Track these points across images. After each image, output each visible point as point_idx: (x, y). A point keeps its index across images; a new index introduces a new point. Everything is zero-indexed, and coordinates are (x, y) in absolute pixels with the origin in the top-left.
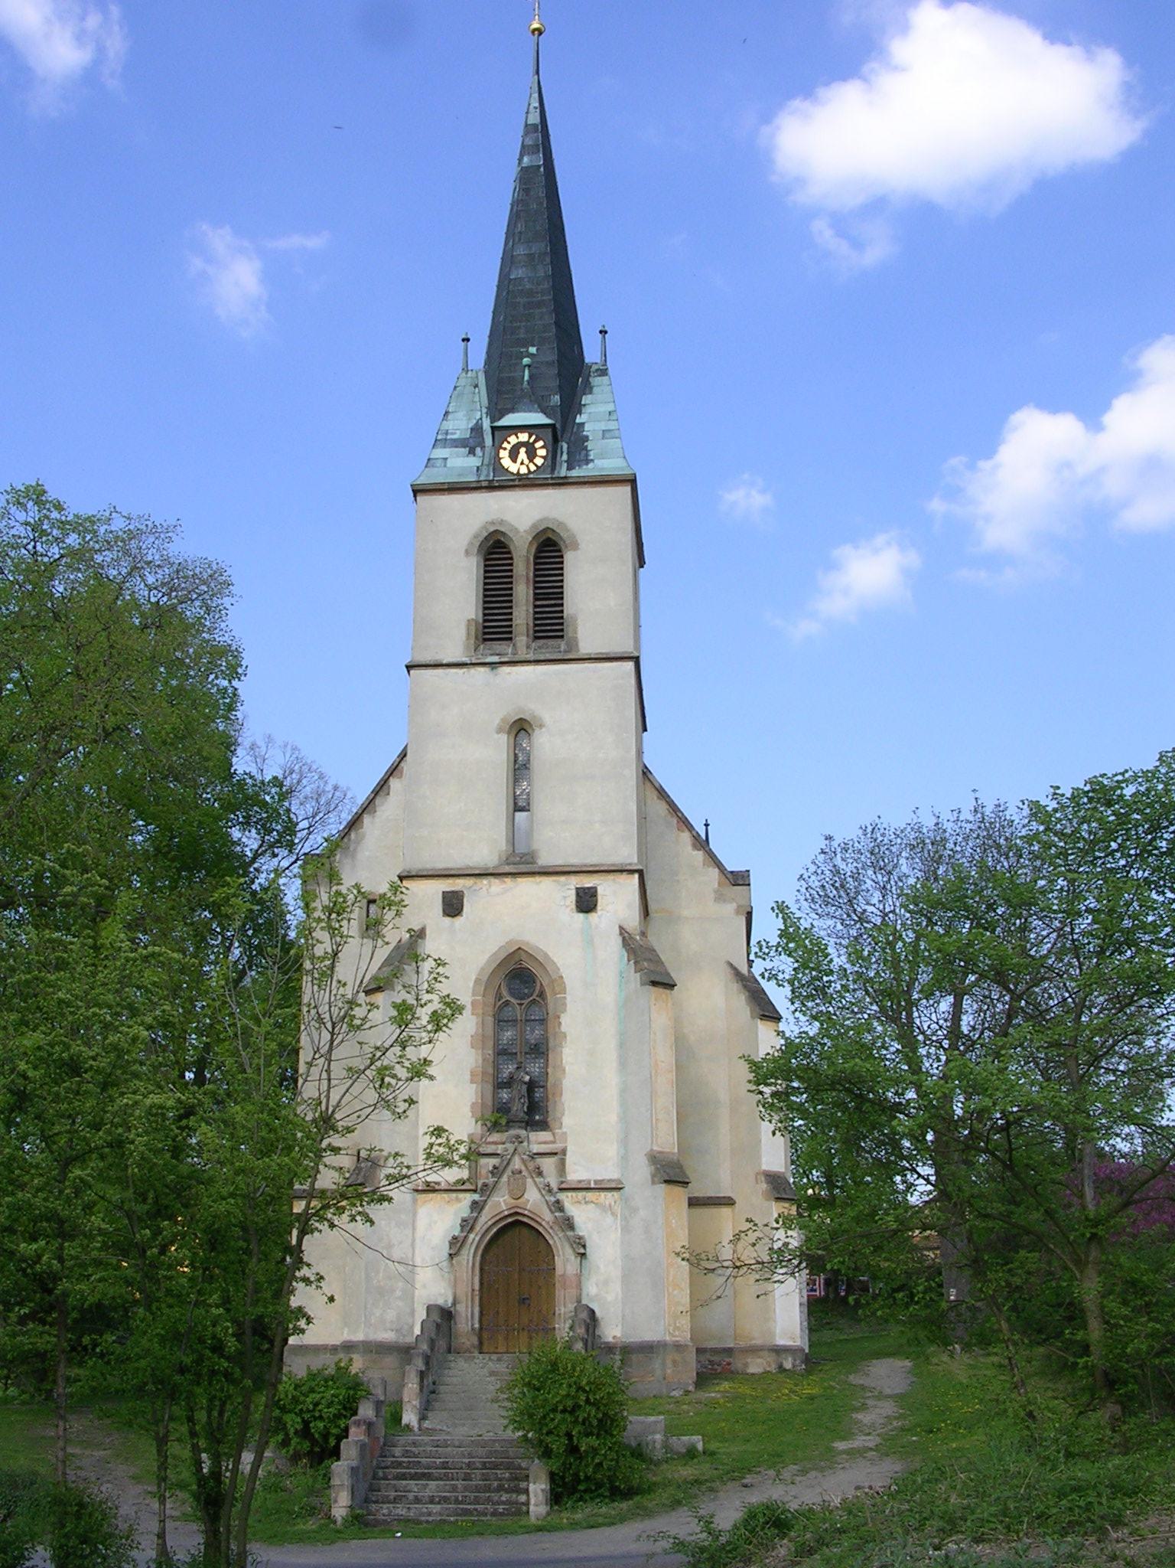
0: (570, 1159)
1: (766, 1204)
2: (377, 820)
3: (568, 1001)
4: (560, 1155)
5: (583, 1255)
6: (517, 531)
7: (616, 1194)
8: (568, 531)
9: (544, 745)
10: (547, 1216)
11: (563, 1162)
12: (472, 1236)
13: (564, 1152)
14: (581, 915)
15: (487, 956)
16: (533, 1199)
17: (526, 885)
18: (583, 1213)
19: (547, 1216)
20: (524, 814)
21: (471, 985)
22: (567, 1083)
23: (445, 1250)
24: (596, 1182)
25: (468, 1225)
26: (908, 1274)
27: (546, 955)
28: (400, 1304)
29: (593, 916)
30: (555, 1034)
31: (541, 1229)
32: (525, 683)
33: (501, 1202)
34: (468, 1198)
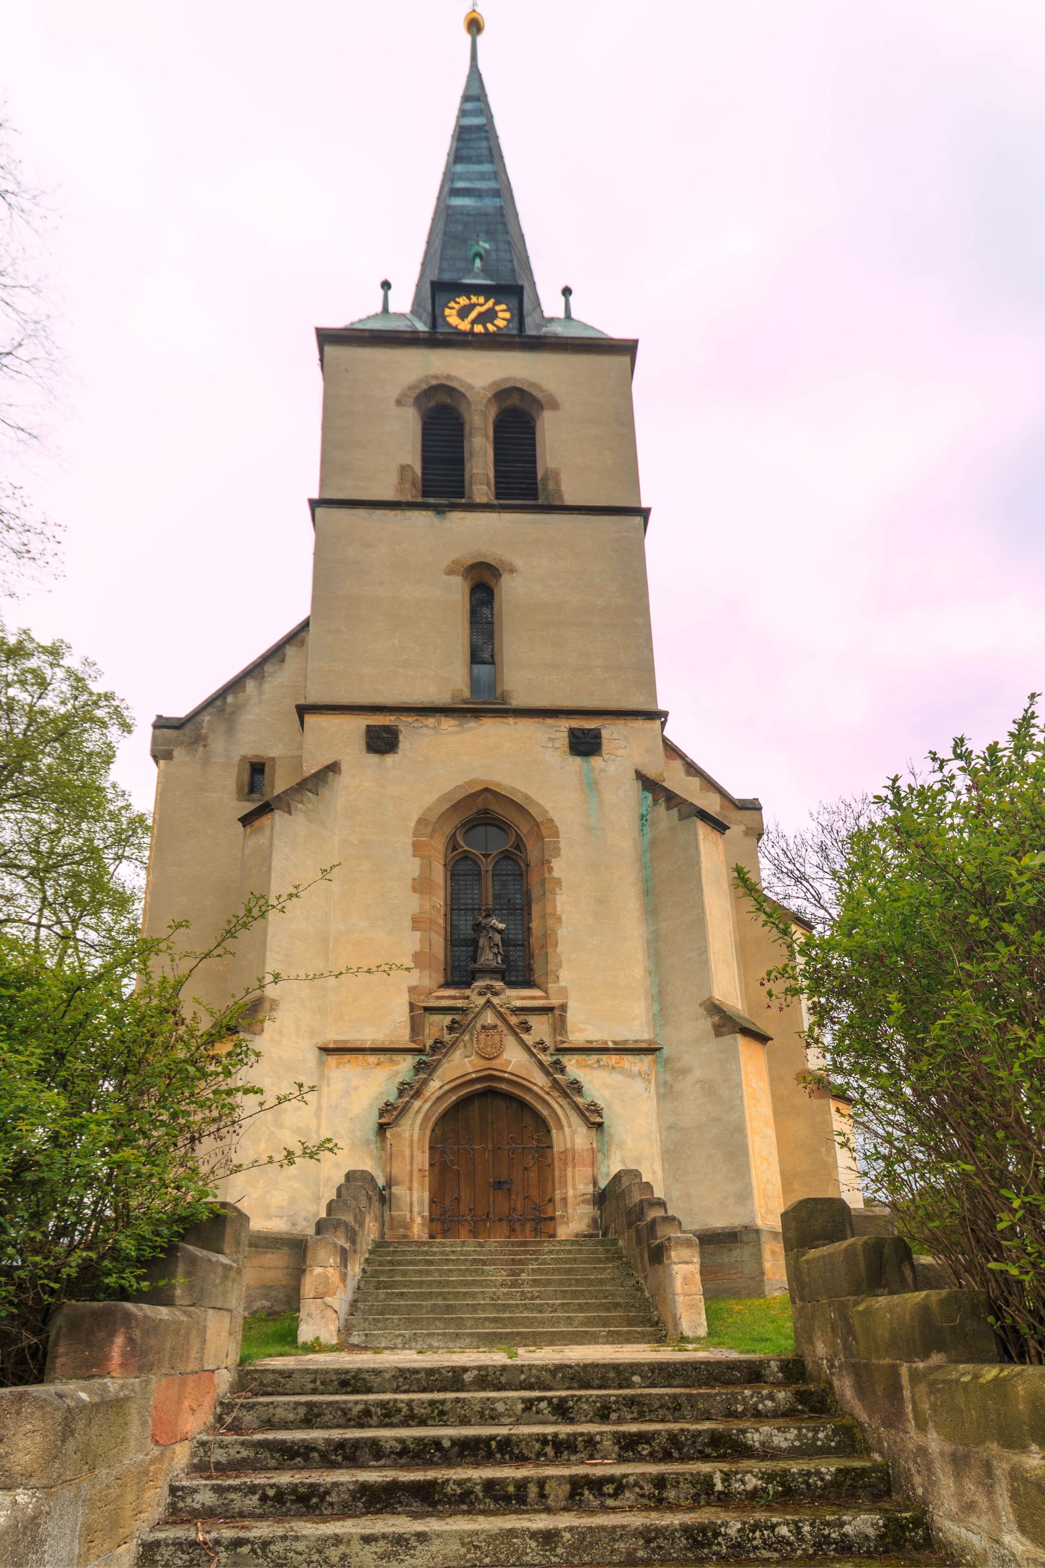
0: (571, 1017)
1: (817, 1102)
2: (267, 686)
3: (562, 845)
4: (556, 1014)
5: (600, 1126)
6: (471, 387)
7: (647, 1059)
8: (543, 391)
9: (511, 591)
10: (540, 1080)
11: (563, 1019)
12: (417, 1104)
13: (563, 1007)
14: (578, 760)
15: (436, 796)
16: (514, 1059)
17: (490, 729)
18: (597, 1081)
19: (540, 1080)
20: (487, 667)
21: (412, 824)
22: (563, 933)
23: (373, 1120)
24: (614, 1042)
25: (410, 1091)
26: (267, 1321)
27: (527, 797)
28: (295, 1185)
29: (596, 761)
30: (543, 882)
31: (528, 1098)
32: (482, 531)
33: (460, 1064)
34: (405, 1065)
